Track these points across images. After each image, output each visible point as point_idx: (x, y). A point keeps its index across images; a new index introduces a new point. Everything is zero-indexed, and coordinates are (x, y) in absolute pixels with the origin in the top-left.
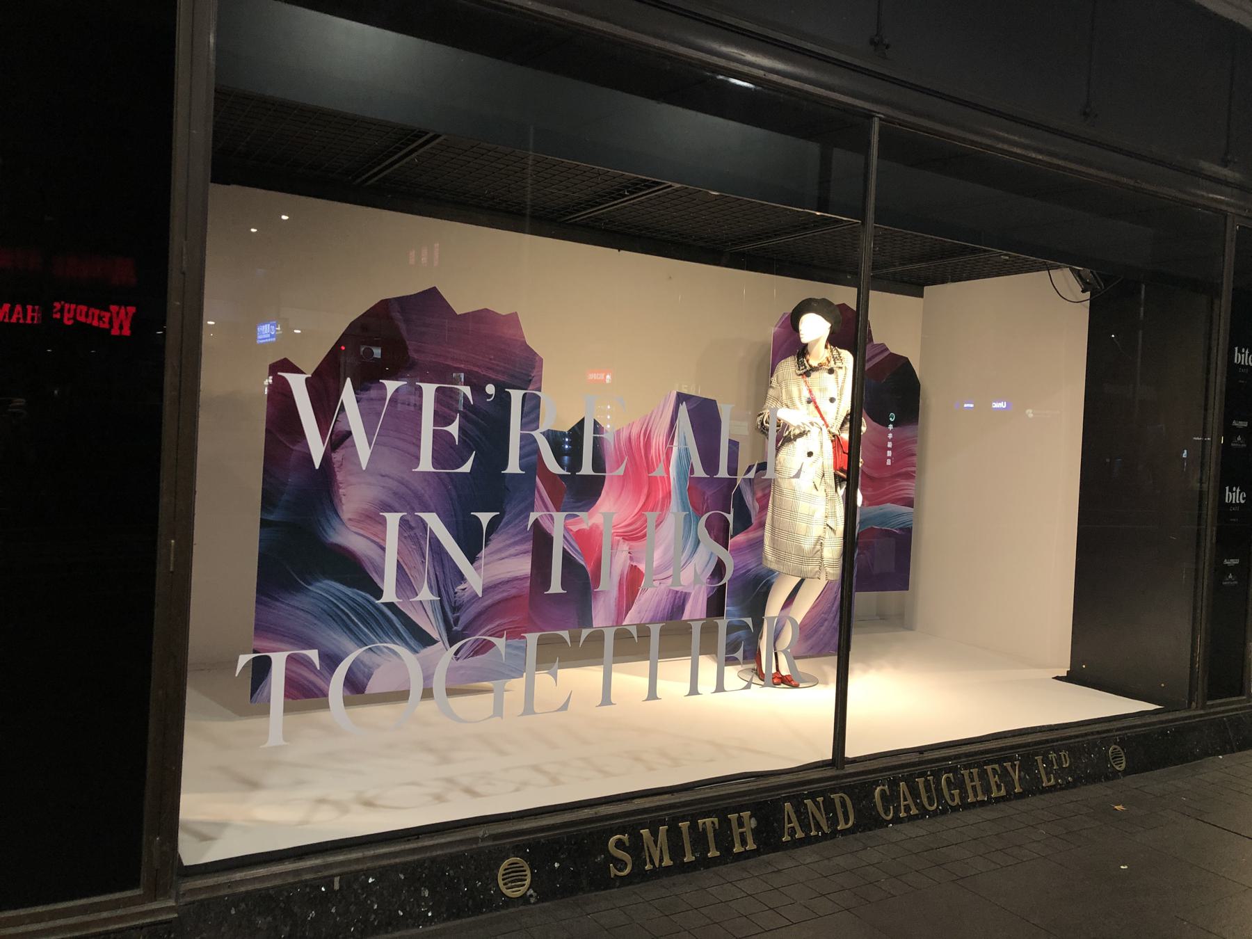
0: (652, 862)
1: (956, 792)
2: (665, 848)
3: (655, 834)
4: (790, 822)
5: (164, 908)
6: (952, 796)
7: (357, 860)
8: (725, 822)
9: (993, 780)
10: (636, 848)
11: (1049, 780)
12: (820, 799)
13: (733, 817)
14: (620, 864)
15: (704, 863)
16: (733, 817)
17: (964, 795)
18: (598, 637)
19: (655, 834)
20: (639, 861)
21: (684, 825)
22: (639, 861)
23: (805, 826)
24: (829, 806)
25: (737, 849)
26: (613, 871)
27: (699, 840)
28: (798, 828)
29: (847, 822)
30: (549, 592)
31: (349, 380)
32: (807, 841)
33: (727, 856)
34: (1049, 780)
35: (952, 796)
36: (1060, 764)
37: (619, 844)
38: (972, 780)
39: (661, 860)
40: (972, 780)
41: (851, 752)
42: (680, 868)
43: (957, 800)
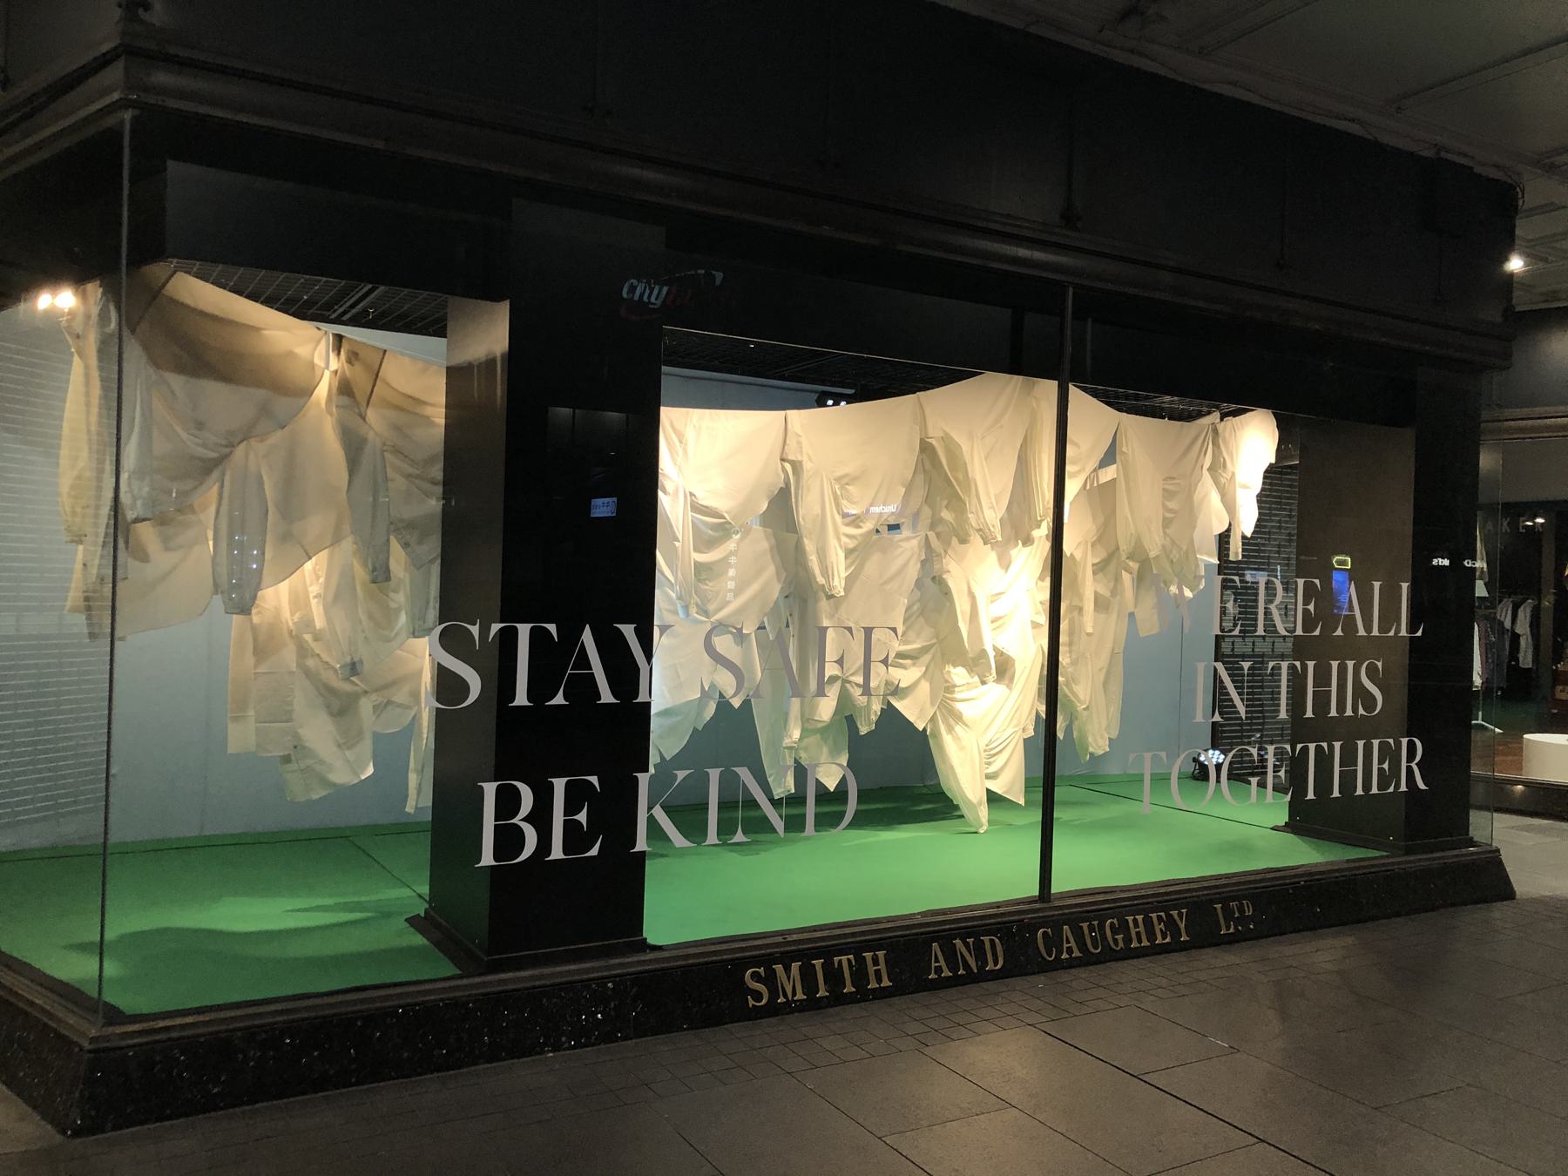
0: (785, 995)
1: (1119, 937)
2: (798, 978)
3: (787, 969)
4: (937, 960)
5: (632, 963)
6: (1115, 941)
7: (532, 978)
8: (861, 961)
9: (1159, 927)
10: (770, 980)
11: (1228, 928)
12: (970, 940)
13: (868, 955)
14: (758, 996)
15: (838, 999)
16: (868, 955)
17: (1128, 940)
18: (842, 815)
19: (787, 969)
20: (774, 994)
21: (818, 963)
22: (774, 994)
23: (953, 967)
24: (979, 947)
25: (873, 985)
26: (751, 1002)
27: (834, 977)
28: (945, 968)
29: (996, 963)
30: (515, 704)
31: (587, 631)
32: (955, 982)
33: (863, 995)
34: (1228, 928)
35: (1115, 941)
36: (1241, 910)
37: (755, 976)
38: (1138, 934)
39: (794, 993)
40: (1138, 934)
41: (1057, 887)
42: (812, 1005)
43: (1121, 944)
